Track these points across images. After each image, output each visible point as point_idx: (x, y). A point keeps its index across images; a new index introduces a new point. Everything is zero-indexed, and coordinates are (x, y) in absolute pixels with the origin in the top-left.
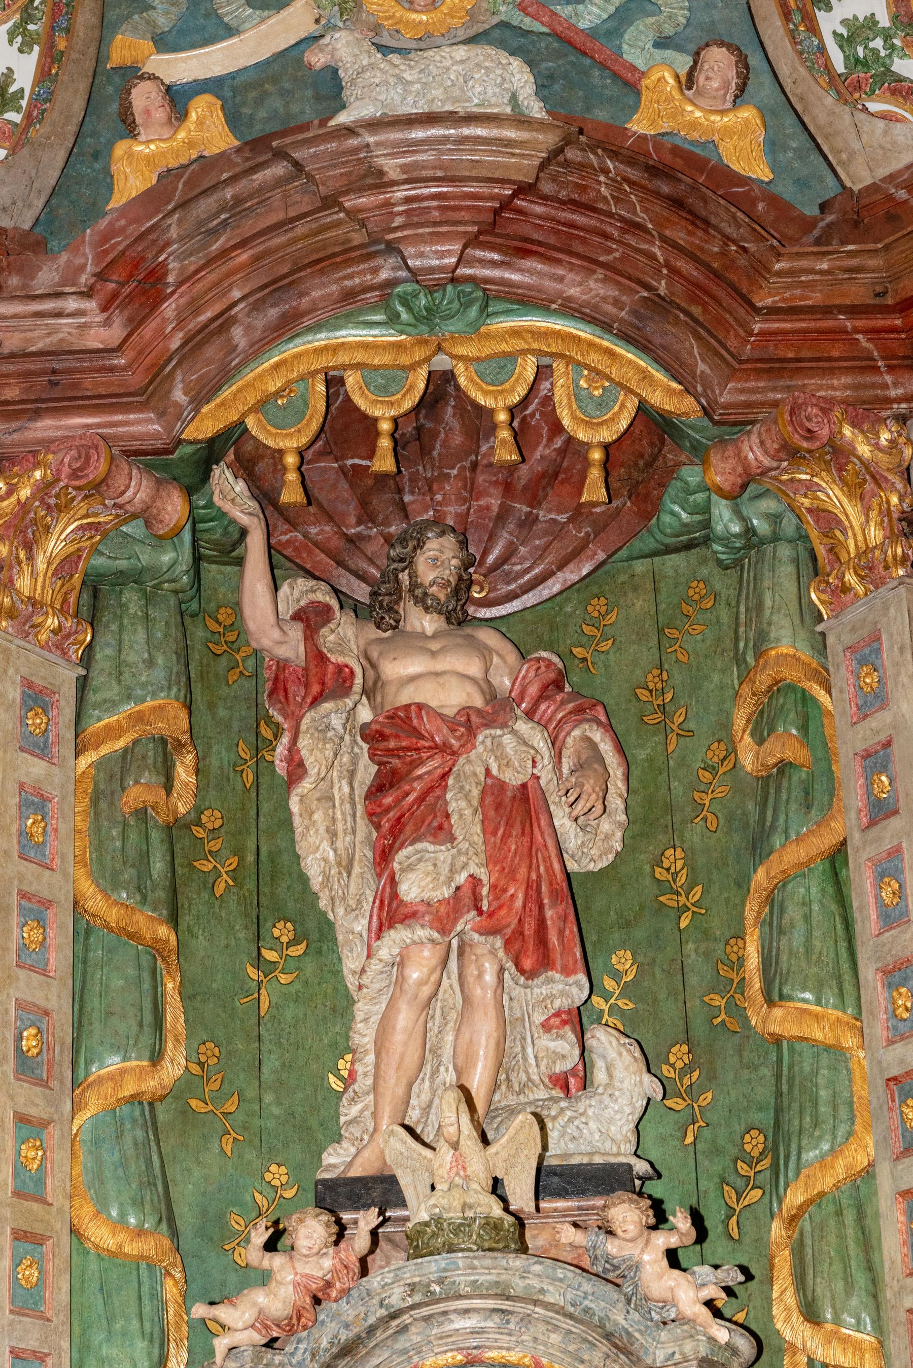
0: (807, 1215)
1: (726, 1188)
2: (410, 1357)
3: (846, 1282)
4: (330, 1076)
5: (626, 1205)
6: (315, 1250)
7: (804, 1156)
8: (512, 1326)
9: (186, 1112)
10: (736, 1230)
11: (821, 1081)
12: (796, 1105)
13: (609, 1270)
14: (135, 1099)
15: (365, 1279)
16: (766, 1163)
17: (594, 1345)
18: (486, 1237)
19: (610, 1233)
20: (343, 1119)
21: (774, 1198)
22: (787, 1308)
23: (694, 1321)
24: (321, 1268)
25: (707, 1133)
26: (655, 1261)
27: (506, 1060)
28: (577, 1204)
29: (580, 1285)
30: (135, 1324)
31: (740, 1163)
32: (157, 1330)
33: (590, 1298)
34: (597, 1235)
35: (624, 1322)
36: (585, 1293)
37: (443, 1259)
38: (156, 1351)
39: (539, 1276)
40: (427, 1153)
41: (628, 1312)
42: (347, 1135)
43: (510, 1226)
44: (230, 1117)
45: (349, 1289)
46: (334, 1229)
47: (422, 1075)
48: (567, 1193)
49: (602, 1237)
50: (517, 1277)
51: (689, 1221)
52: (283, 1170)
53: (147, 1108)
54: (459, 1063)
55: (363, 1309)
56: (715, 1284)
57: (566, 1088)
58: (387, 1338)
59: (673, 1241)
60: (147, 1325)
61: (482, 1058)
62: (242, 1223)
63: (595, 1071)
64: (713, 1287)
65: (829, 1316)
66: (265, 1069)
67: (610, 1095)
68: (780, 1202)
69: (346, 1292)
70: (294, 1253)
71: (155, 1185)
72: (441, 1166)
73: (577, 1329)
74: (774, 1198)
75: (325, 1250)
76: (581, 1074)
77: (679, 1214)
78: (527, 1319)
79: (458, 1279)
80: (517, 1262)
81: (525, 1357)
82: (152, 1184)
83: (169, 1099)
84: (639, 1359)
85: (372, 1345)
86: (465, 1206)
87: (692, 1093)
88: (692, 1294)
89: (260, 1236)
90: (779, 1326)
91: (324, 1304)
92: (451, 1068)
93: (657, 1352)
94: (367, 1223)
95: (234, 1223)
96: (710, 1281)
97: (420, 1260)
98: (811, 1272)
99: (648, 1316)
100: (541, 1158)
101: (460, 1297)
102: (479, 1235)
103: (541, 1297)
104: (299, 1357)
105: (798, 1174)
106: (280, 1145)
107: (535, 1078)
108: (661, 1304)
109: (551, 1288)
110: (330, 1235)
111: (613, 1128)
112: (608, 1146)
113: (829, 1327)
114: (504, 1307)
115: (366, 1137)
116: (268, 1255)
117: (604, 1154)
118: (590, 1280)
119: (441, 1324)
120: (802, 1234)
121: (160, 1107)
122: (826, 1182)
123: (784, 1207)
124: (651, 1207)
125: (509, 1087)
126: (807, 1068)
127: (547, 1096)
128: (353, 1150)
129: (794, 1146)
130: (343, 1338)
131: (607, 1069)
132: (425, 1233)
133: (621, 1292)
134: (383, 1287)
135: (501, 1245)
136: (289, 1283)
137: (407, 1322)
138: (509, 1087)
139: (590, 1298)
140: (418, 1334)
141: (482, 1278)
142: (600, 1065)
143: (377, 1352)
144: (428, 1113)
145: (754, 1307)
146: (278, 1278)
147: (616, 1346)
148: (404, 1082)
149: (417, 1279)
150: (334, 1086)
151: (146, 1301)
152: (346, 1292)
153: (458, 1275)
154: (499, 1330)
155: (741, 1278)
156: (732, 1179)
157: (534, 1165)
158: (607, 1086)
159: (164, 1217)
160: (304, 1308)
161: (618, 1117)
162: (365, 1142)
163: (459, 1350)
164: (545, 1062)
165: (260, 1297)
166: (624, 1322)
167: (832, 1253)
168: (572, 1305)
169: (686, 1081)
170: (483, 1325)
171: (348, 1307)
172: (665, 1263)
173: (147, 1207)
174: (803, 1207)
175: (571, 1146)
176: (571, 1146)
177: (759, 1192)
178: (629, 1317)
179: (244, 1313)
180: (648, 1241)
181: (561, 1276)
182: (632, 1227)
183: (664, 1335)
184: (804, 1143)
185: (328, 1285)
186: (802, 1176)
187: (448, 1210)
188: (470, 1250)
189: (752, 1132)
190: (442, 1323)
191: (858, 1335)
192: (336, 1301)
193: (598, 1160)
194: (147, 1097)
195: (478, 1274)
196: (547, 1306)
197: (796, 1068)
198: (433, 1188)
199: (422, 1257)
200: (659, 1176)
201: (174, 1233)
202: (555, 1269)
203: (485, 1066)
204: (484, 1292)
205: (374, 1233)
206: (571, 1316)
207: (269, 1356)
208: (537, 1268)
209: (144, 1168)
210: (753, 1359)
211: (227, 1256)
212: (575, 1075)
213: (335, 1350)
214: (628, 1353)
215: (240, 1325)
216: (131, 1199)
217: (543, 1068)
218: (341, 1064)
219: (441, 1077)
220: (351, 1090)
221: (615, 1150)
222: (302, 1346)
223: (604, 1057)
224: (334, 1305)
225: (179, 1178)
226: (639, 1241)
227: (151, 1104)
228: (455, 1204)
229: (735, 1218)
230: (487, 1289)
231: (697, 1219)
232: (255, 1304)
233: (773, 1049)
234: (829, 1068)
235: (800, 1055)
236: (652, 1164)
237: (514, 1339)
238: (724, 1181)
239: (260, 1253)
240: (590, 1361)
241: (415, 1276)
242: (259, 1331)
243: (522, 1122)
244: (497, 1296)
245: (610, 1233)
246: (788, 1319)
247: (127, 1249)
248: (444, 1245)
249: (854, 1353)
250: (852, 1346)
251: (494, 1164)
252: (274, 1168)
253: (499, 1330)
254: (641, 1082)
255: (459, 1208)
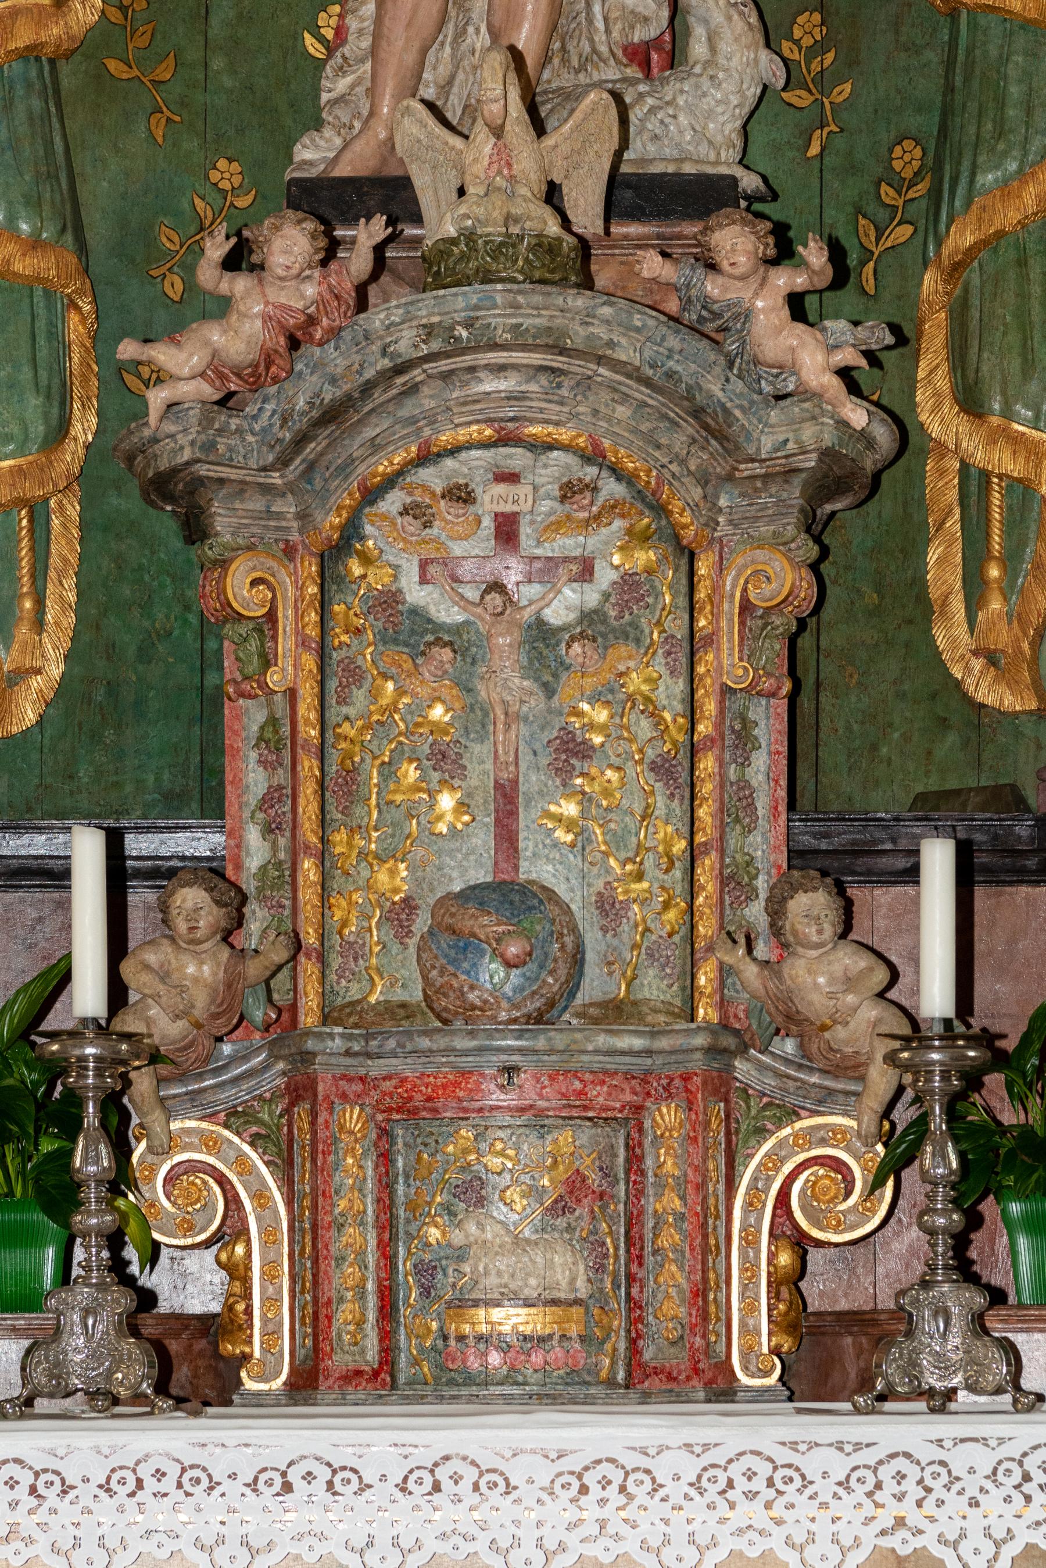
0: (976, 264)
1: (862, 221)
2: (420, 429)
3: (1025, 360)
4: (306, 35)
5: (737, 228)
6: (294, 271)
7: (980, 179)
8: (564, 392)
9: (100, 78)
10: (872, 281)
11: (1012, 71)
12: (973, 107)
13: (705, 319)
14: (30, 53)
15: (362, 316)
16: (921, 188)
17: (677, 424)
18: (537, 264)
19: (712, 267)
20: (325, 97)
21: (931, 238)
22: (937, 394)
23: (820, 396)
24: (302, 297)
25: (840, 142)
26: (773, 309)
27: (563, 21)
28: (656, 230)
29: (663, 338)
30: (26, 374)
31: (884, 187)
32: (56, 381)
33: (676, 357)
34: (693, 269)
35: (720, 394)
36: (670, 350)
37: (475, 292)
38: (55, 411)
39: (608, 322)
40: (457, 142)
41: (727, 380)
42: (330, 119)
43: (571, 250)
44: (162, 87)
45: (340, 329)
46: (323, 243)
47: (441, 37)
48: (644, 214)
49: (700, 271)
50: (577, 322)
51: (826, 253)
52: (235, 167)
53: (47, 68)
54: (497, 21)
55: (357, 358)
56: (854, 346)
57: (646, 66)
58: (389, 401)
59: (800, 281)
60: (43, 375)
61: (529, 16)
62: (176, 239)
63: (692, 41)
64: (851, 349)
65: (997, 406)
66: (215, 21)
67: (712, 78)
68: (939, 244)
69: (334, 333)
70: (264, 274)
71: (58, 179)
72: (476, 160)
73: (654, 400)
74: (931, 238)
75: (307, 272)
76: (668, 47)
77: (812, 244)
78: (585, 384)
79: (493, 321)
80: (579, 301)
81: (579, 436)
82: (52, 176)
83: (77, 57)
84: (738, 447)
85: (366, 409)
86: (509, 219)
87: (823, 83)
88: (820, 358)
89: (217, 248)
90: (923, 418)
91: (303, 349)
92: (483, 28)
93: (763, 438)
94: (370, 236)
95: (164, 240)
96: (847, 342)
97: (442, 292)
98: (976, 343)
99: (756, 387)
100: (618, 155)
101: (495, 347)
102: (527, 260)
103: (609, 352)
104: (264, 420)
105: (968, 204)
106: (232, 132)
107: (603, 49)
108: (775, 371)
109: (624, 341)
110: (317, 251)
111: (711, 126)
112: (703, 150)
113: (995, 420)
114: (555, 365)
115: (357, 125)
116: (228, 275)
117: (698, 162)
118: (677, 332)
119: (465, 384)
120: (966, 290)
121: (64, 69)
122: (1008, 217)
123: (945, 251)
124: (772, 232)
125: (565, 61)
126: (994, 52)
127: (618, 76)
128: (338, 142)
129: (966, 164)
130: (328, 397)
131: (709, 39)
132: (450, 253)
133: (721, 351)
134: (388, 328)
135: (557, 277)
136: (256, 315)
137: (418, 379)
138: (565, 61)
139: (676, 357)
140: (431, 397)
141: (528, 322)
142: (699, 31)
143: (374, 419)
144: (448, 94)
145: (890, 390)
146: (242, 308)
147: (706, 427)
148: (416, 45)
149: (436, 319)
150: (311, 50)
151: (41, 341)
152: (334, 333)
153: (495, 316)
154: (547, 396)
155: (890, 340)
156: (871, 208)
157: (607, 167)
158: (707, 64)
159: (69, 225)
160: (276, 351)
161: (720, 109)
162: (356, 131)
163: (489, 421)
164: (619, 26)
165: (215, 335)
166: (720, 394)
167: (1008, 318)
168: (651, 367)
169: (816, 67)
170: (523, 388)
171: (336, 354)
172: (786, 313)
173: (46, 207)
174: (971, 252)
175: (652, 148)
176: (652, 148)
177: (908, 230)
178: (729, 387)
179: (191, 355)
180: (764, 281)
181: (639, 324)
182: (743, 259)
183: (774, 415)
184: (981, 159)
185: (312, 321)
186: (974, 207)
187: (485, 223)
188: (514, 280)
189: (905, 143)
190: (467, 383)
191: (1035, 433)
192: (321, 344)
193: (688, 169)
194: (49, 50)
195: (522, 315)
196: (616, 365)
197: (978, 52)
198: (461, 192)
199: (444, 287)
200: (775, 197)
201: (82, 248)
202: (630, 314)
203: (533, 27)
204: (530, 341)
205: (379, 250)
206: (647, 382)
207: (223, 418)
208: (606, 311)
209: (41, 153)
210: (891, 457)
211: (154, 285)
212: (659, 50)
213: (315, 413)
214: (721, 437)
215: (186, 372)
216: (24, 196)
217: (615, 34)
218: (322, 19)
219: (469, 41)
220: (339, 54)
221: (712, 157)
222: (269, 407)
223: (706, 22)
224: (317, 351)
225: (89, 170)
226: (751, 280)
227: (52, 62)
228: (496, 214)
229: (871, 264)
230: (535, 337)
231: (837, 253)
232: (207, 343)
233: (944, 23)
234: (1026, 54)
235: (985, 33)
236: (765, 179)
237: (566, 409)
238: (859, 211)
239: (217, 272)
240: (669, 447)
241: (433, 314)
242: (211, 383)
243: (594, 103)
244: (548, 348)
245: (712, 267)
246: (936, 409)
247: (18, 267)
248: (477, 271)
249: (1027, 460)
250: (1026, 448)
251: (551, 162)
252: (222, 164)
253: (547, 396)
254: (756, 61)
255: (500, 220)
